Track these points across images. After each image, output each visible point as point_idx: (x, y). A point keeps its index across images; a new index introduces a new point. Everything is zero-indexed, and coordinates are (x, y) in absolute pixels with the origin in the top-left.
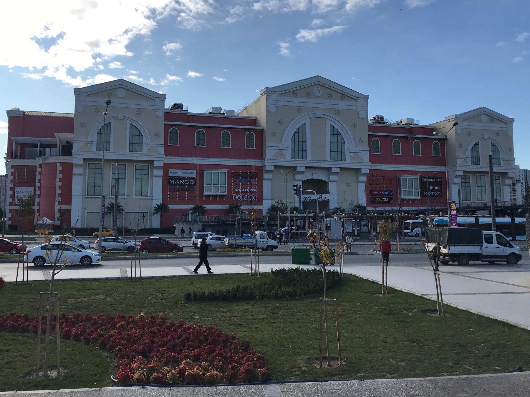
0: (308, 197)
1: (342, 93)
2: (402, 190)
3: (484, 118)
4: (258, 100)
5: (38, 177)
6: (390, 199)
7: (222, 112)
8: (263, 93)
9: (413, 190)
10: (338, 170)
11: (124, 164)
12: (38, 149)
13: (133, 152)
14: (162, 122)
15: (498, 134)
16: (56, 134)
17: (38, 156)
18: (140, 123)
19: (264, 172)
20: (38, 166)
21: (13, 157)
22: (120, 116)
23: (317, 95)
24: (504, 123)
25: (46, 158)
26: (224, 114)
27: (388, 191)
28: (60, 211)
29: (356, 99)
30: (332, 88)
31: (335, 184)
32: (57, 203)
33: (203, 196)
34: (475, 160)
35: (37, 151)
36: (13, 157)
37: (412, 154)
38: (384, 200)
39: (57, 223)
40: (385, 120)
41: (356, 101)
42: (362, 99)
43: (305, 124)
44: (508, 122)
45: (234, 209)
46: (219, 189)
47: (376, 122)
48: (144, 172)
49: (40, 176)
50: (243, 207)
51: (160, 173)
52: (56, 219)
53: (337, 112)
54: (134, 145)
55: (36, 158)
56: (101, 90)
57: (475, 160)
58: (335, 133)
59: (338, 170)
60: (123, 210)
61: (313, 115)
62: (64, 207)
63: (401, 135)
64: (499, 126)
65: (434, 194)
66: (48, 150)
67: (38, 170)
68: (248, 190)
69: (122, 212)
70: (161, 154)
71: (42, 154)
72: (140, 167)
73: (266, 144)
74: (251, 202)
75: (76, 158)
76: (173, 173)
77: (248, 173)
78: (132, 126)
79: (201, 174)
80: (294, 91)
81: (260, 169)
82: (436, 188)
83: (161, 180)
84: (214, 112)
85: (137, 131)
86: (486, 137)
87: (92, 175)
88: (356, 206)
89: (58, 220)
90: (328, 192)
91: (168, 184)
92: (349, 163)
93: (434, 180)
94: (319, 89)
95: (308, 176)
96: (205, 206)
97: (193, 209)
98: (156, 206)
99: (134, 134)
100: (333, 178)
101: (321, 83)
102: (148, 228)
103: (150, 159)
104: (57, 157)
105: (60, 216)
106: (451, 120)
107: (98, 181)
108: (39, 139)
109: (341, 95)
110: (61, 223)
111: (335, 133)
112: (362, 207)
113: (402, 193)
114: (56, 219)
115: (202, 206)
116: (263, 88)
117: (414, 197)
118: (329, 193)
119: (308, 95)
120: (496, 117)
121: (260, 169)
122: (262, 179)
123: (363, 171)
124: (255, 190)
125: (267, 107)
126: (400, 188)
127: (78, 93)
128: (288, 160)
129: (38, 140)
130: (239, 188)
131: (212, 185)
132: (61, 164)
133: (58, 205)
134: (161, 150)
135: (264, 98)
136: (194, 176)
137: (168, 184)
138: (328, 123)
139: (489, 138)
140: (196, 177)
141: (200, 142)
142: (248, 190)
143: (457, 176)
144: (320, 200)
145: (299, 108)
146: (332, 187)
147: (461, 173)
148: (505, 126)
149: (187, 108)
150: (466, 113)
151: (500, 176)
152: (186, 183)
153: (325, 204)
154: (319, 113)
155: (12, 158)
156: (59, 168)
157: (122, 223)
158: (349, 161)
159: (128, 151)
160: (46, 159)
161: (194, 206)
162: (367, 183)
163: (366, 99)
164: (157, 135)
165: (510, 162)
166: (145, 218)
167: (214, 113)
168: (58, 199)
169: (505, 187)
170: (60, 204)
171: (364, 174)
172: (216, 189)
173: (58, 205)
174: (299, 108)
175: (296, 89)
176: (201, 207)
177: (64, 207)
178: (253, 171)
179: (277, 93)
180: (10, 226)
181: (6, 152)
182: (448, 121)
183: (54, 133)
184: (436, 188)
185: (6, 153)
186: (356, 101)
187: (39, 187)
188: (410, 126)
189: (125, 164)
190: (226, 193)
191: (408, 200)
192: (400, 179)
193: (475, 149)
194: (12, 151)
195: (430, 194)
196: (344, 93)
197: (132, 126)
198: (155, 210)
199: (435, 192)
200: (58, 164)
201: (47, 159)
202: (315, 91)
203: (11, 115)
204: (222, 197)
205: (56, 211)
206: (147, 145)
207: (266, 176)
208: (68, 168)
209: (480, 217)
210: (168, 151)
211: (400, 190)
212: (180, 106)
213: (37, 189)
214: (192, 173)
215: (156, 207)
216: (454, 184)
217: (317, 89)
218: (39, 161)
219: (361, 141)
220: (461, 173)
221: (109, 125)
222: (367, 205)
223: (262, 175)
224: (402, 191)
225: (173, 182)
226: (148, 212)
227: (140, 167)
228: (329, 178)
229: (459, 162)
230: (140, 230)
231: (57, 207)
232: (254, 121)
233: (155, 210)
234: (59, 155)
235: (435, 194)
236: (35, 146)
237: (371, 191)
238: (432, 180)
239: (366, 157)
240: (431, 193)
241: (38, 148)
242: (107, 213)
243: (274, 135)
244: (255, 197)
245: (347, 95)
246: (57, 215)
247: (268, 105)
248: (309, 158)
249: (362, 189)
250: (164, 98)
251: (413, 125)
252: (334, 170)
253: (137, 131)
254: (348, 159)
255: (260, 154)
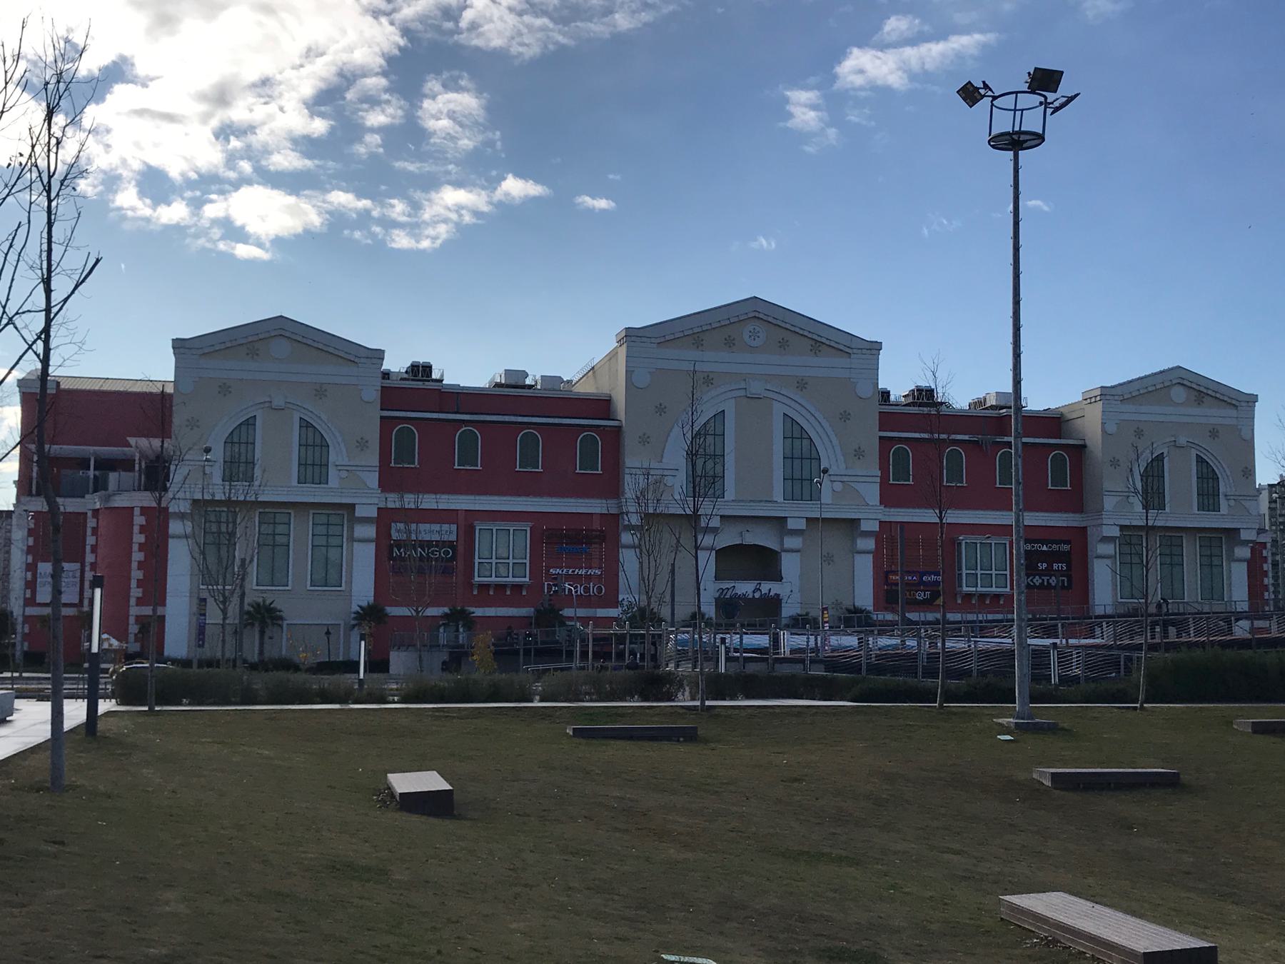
0: (728, 589)
1: (815, 337)
2: (964, 572)
3: (1179, 394)
4: (612, 355)
5: (90, 540)
6: (935, 595)
7: (528, 381)
8: (620, 340)
9: (994, 572)
10: (802, 525)
11: (287, 511)
12: (91, 473)
13: (306, 485)
14: (376, 414)
15: (1214, 433)
16: (132, 441)
17: (91, 490)
18: (323, 416)
19: (621, 528)
20: (90, 514)
21: (34, 492)
22: (278, 401)
23: (754, 344)
24: (1232, 406)
25: (110, 496)
26: (530, 387)
27: (930, 574)
28: (139, 619)
29: (1237, 404)
30: (788, 326)
31: (796, 556)
32: (133, 601)
33: (471, 585)
34: (1153, 495)
35: (89, 477)
36: (34, 492)
37: (996, 484)
38: (920, 596)
39: (134, 647)
40: (435, 375)
41: (850, 357)
42: (864, 351)
43: (722, 414)
44: (1243, 404)
45: (548, 616)
46: (511, 569)
47: (913, 404)
48: (333, 530)
49: (95, 537)
50: (567, 612)
51: (370, 531)
52: (131, 638)
53: (802, 385)
54: (310, 469)
55: (87, 496)
56: (235, 343)
57: (1153, 495)
58: (795, 433)
59: (802, 525)
60: (281, 618)
61: (742, 393)
62: (147, 611)
63: (966, 437)
64: (1215, 415)
65: (1051, 581)
66: (113, 477)
67: (91, 523)
68: (582, 572)
69: (280, 622)
70: (371, 489)
71: (100, 485)
72: (324, 519)
73: (624, 463)
74: (585, 601)
75: (179, 497)
76: (397, 531)
77: (563, 530)
78: (251, 421)
79: (470, 531)
80: (696, 336)
81: (613, 520)
82: (1055, 566)
83: (371, 548)
84: (508, 382)
85: (317, 434)
86: (1182, 440)
87: (322, 541)
88: (849, 611)
89: (136, 641)
90: (778, 578)
91: (391, 557)
92: (830, 502)
93: (1033, 547)
94: (757, 329)
95: (728, 538)
96: (472, 609)
97: (446, 616)
98: (358, 609)
99: (310, 441)
100: (791, 542)
101: (761, 316)
102: (341, 659)
103: (344, 501)
104: (134, 494)
105: (139, 632)
106: (1093, 400)
107: (333, 554)
108: (92, 449)
109: (813, 343)
110: (142, 647)
111: (795, 433)
112: (861, 611)
113: (964, 581)
114: (131, 638)
115: (466, 610)
116: (619, 327)
117: (994, 589)
118: (780, 579)
119: (730, 343)
120: (1210, 392)
121: (613, 520)
122: (617, 544)
123: (865, 526)
124: (600, 573)
125: (629, 373)
126: (960, 569)
127: (182, 350)
128: (675, 499)
129: (91, 450)
130: (561, 568)
131: (994, 572)
132: (144, 511)
133: (137, 605)
134: (373, 479)
135: (623, 352)
136: (453, 538)
137: (391, 557)
138: (778, 410)
139: (1190, 445)
140: (457, 542)
141: (467, 458)
142: (582, 572)
143: (1106, 539)
144: (757, 595)
145: (708, 376)
146: (790, 564)
147: (1116, 532)
148: (1233, 413)
149: (442, 375)
150: (1146, 377)
151: (1184, 535)
152: (433, 554)
153: (773, 604)
154: (756, 388)
155: (30, 494)
156: (139, 520)
157: (281, 646)
158: (831, 502)
159: (295, 483)
160: (108, 499)
161: (446, 610)
162: (877, 554)
163: (874, 352)
164: (362, 444)
165: (1247, 504)
166: (331, 637)
167: (507, 386)
168: (136, 592)
169: (1235, 566)
170: (140, 602)
171: (867, 534)
172: (502, 570)
173: (137, 605)
174: (708, 376)
175: (700, 330)
176: (463, 612)
177: (147, 611)
178: (596, 526)
179: (653, 340)
180: (26, 655)
181: (17, 479)
182: (1089, 401)
183: (128, 438)
184: (1055, 566)
185: (15, 482)
186: (850, 357)
187: (92, 564)
188: (1001, 411)
189: (290, 511)
190: (527, 579)
191: (982, 596)
192: (960, 544)
193: (1154, 473)
194: (31, 479)
195: (1040, 581)
196: (819, 339)
197: (305, 425)
198: (355, 619)
199: (1037, 577)
200: (137, 512)
201: (112, 498)
202: (746, 337)
203: (29, 390)
204: (517, 588)
205: (132, 620)
206: (339, 468)
207: (626, 538)
208: (158, 520)
209: (97, 538)
210: (389, 481)
211: (960, 572)
212: (424, 371)
213: (87, 568)
214: (448, 532)
215: (357, 613)
216: (798, 551)
217: (751, 328)
218: (94, 501)
219: (859, 454)
220: (1116, 532)
221: (251, 421)
222: (877, 607)
223: (618, 536)
224: (964, 575)
225: (401, 553)
226: (342, 623)
227: (324, 519)
228: (782, 543)
229: (1109, 503)
230: (320, 664)
231: (134, 611)
232: (602, 406)
233: (355, 619)
234: (139, 490)
235: (1053, 581)
236: (83, 463)
237: (887, 574)
238: (1045, 548)
239: (872, 492)
240: (1043, 580)
241: (89, 470)
242: (246, 626)
243: (644, 440)
244: (600, 589)
245: (828, 342)
246: (133, 628)
247: (632, 369)
248: (729, 495)
249: (865, 568)
250: (379, 358)
251: (1004, 410)
252: (791, 524)
253: (317, 434)
254: (826, 497)
255: (611, 485)
